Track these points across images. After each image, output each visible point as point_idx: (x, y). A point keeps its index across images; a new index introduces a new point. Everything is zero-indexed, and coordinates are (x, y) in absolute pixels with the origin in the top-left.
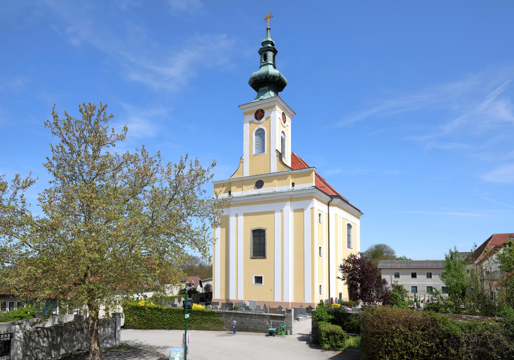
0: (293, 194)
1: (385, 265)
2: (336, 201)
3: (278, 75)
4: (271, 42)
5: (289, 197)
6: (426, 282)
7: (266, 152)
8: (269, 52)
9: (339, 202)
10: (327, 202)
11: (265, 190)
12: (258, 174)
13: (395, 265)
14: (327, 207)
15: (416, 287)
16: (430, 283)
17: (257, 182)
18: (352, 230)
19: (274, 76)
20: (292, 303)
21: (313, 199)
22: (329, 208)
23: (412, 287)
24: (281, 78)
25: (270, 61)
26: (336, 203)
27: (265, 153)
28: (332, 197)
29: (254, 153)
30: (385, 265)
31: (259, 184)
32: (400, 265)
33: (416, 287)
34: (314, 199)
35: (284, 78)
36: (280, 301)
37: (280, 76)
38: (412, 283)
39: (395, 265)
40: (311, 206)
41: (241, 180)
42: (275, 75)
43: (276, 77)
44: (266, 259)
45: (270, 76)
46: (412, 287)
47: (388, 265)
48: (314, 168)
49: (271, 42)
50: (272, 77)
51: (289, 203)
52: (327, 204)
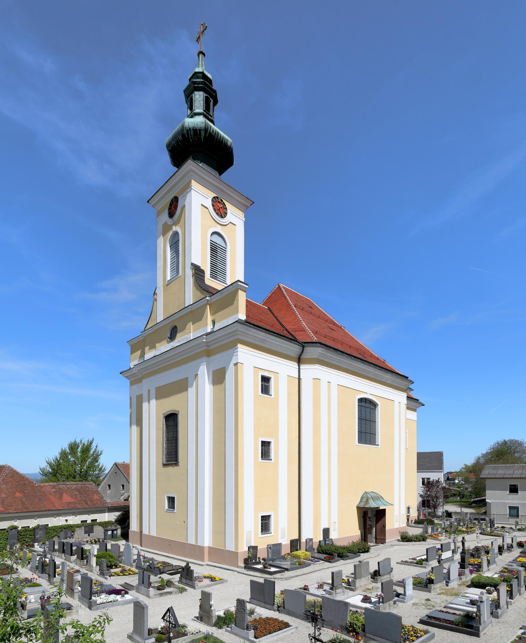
0: (209, 340)
1: (494, 472)
2: (311, 352)
3: (203, 126)
4: (201, 75)
5: (204, 348)
6: (508, 499)
7: (180, 274)
8: (196, 93)
9: (320, 353)
10: (295, 355)
11: (179, 341)
12: (168, 317)
13: (511, 472)
14: (295, 365)
15: (517, 508)
16: (515, 502)
17: (171, 331)
18: (378, 411)
19: (196, 130)
20: (209, 548)
21: (237, 345)
22: (301, 367)
23: (510, 508)
24: (210, 133)
25: (199, 108)
26: (316, 357)
27: (179, 275)
28: (303, 345)
29: (169, 278)
30: (494, 472)
31: (173, 334)
32: (520, 472)
33: (517, 508)
34: (239, 346)
35: (221, 132)
36: (194, 544)
37: (206, 129)
38: (509, 501)
39: (511, 472)
40: (233, 362)
41: (153, 331)
42: (196, 126)
43: (200, 130)
44: (179, 466)
45: (188, 130)
46: (510, 508)
47: (500, 472)
48: (239, 283)
49: (201, 75)
50: (192, 132)
51: (205, 359)
52: (297, 360)
